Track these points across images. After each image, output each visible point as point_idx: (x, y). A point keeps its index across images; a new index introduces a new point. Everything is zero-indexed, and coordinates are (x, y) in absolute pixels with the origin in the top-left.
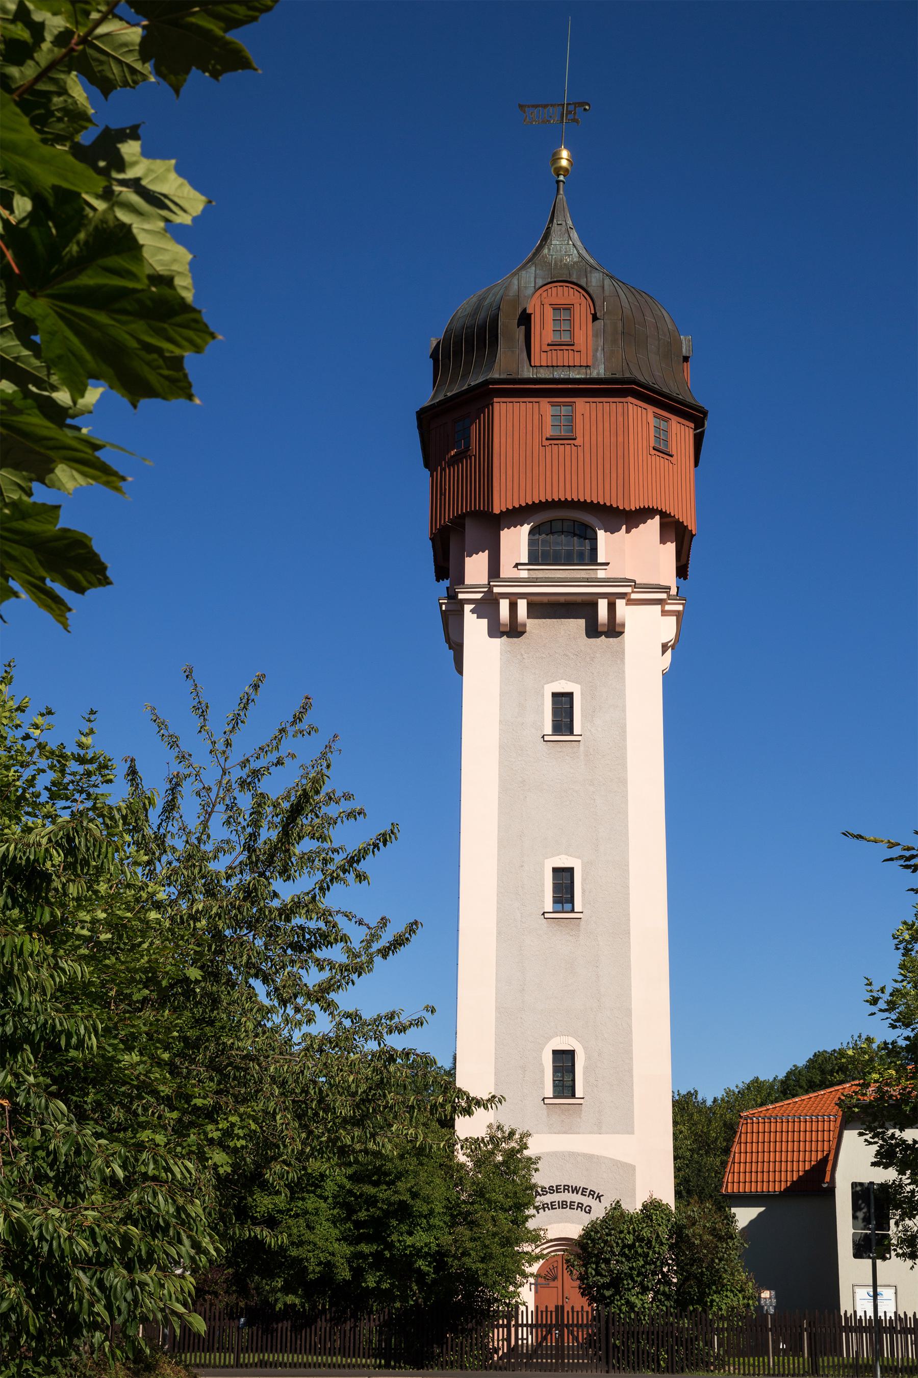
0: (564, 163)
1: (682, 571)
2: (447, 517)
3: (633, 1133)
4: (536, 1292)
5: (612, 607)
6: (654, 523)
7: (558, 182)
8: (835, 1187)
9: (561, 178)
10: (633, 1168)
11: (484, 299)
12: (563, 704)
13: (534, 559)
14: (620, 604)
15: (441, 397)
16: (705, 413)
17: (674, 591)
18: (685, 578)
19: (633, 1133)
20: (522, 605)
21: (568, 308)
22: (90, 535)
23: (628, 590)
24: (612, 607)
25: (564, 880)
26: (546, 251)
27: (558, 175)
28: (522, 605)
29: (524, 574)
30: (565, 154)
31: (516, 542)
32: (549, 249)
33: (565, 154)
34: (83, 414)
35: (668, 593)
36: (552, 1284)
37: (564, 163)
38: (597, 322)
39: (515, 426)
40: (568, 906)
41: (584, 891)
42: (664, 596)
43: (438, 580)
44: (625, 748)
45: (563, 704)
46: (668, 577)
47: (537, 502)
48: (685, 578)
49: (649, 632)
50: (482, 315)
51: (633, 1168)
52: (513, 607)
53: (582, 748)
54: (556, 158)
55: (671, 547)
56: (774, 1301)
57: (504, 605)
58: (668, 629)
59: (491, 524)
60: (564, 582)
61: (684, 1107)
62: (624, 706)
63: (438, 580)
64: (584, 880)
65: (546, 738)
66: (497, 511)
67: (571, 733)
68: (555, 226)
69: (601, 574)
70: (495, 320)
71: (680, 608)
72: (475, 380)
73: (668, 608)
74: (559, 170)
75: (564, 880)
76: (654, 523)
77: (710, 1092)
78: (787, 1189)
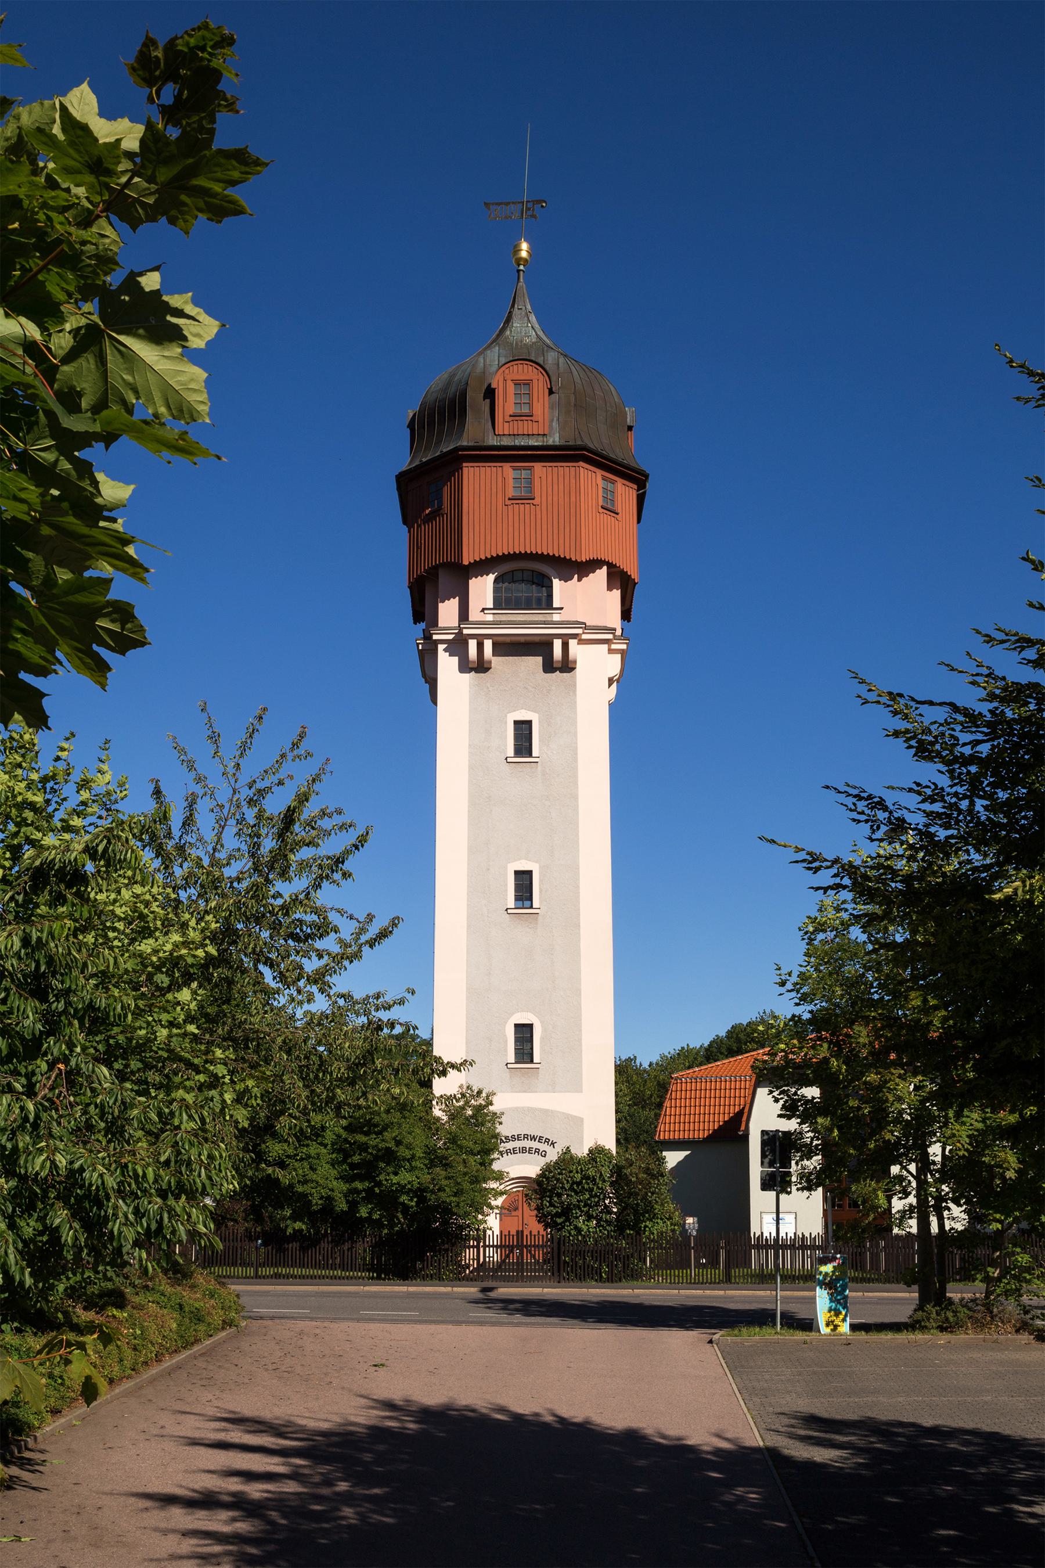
0: (524, 254)
2: (424, 566)
4: (501, 1220)
5: (565, 646)
7: (519, 271)
9: (522, 267)
12: (523, 730)
14: (573, 643)
15: (417, 463)
16: (647, 476)
17: (619, 632)
18: (629, 621)
20: (488, 645)
21: (528, 383)
23: (580, 631)
24: (565, 646)
26: (508, 333)
27: (519, 265)
28: (488, 645)
29: (490, 618)
30: (524, 246)
31: (482, 589)
33: (524, 246)
39: (481, 487)
40: (527, 903)
41: (541, 891)
43: (415, 623)
45: (523, 730)
46: (614, 620)
48: (629, 621)
49: (597, 667)
50: (453, 389)
54: (517, 250)
55: (617, 594)
57: (473, 644)
58: (613, 665)
60: (524, 624)
61: (624, 1071)
63: (415, 623)
64: (541, 881)
65: (509, 760)
66: (466, 562)
69: (556, 617)
71: (624, 647)
72: (446, 447)
73: (613, 646)
74: (519, 261)
77: (647, 1057)
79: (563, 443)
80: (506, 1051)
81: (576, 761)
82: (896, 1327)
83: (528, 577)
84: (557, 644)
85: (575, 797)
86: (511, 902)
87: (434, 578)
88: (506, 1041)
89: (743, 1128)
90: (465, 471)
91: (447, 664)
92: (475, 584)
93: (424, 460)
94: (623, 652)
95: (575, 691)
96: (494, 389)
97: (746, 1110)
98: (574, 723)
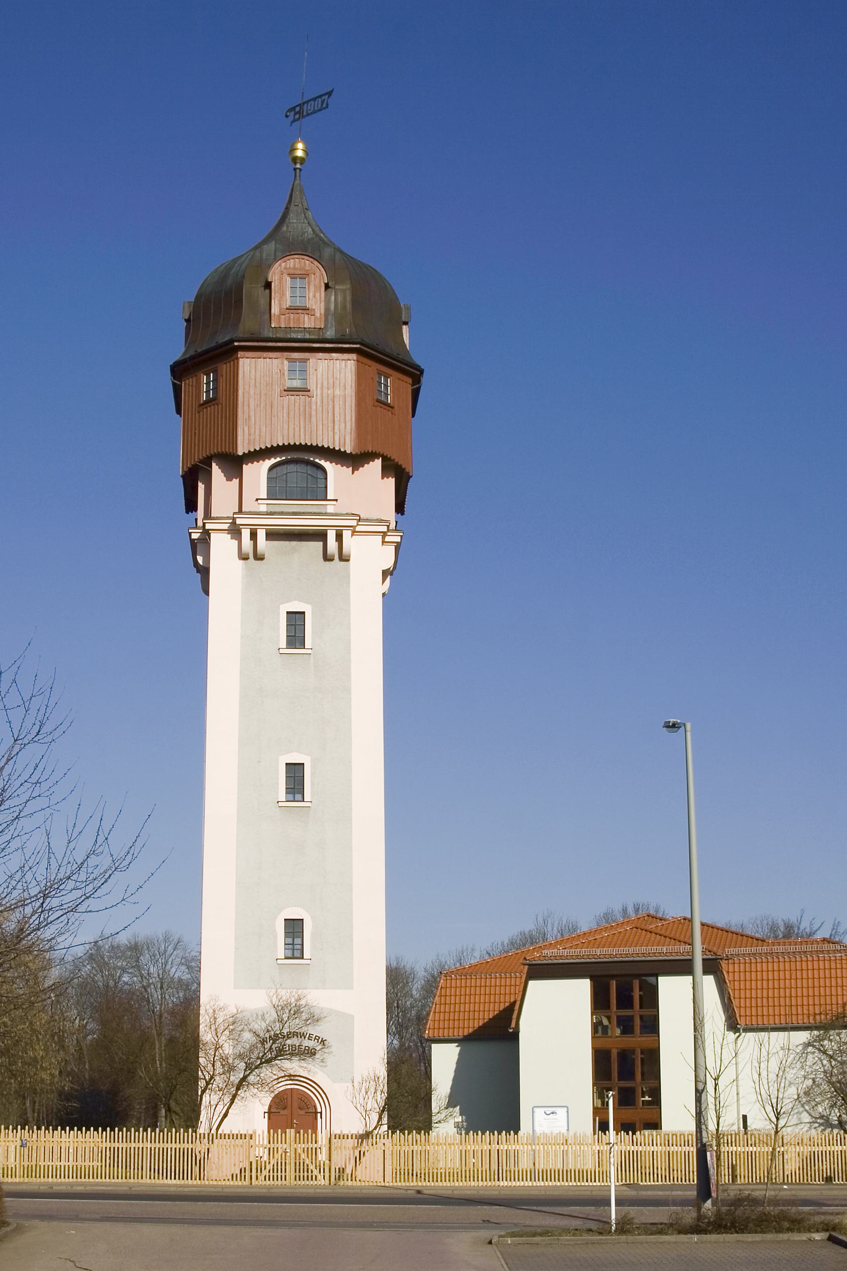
0: (300, 153)
1: (400, 508)
2: (196, 458)
3: (352, 988)
4: (269, 1118)
5: (339, 537)
6: (378, 463)
7: (295, 169)
8: (518, 1032)
9: (298, 166)
10: (352, 1017)
11: (231, 268)
12: (296, 620)
13: (272, 495)
14: (346, 534)
15: (191, 353)
16: (422, 372)
17: (392, 526)
18: (403, 514)
19: (352, 988)
20: (261, 534)
21: (304, 276)
22: (529, 926)
23: (354, 523)
24: (339, 537)
25: (295, 773)
26: (284, 228)
27: (295, 163)
28: (261, 534)
29: (263, 508)
30: (300, 146)
31: (257, 474)
32: (288, 227)
33: (300, 146)
34: (797, 1224)
35: (388, 526)
36: (282, 1112)
37: (300, 153)
38: (329, 290)
39: (255, 372)
40: (298, 797)
41: (312, 784)
42: (384, 529)
43: (187, 512)
44: (350, 661)
45: (296, 620)
46: (390, 514)
47: (275, 445)
48: (403, 514)
49: (371, 556)
50: (230, 281)
51: (352, 1017)
52: (254, 535)
53: (312, 660)
54: (293, 149)
55: (391, 482)
56: (465, 1124)
57: (246, 534)
58: (387, 558)
59: (234, 464)
60: (298, 515)
61: (396, 978)
62: (349, 624)
63: (187, 512)
64: (313, 774)
65: (281, 651)
66: (240, 453)
67: (303, 646)
68: (292, 207)
69: (330, 509)
70: (239, 288)
71: (398, 539)
72: (223, 338)
73: (387, 539)
74: (295, 159)
75: (295, 773)
76: (378, 463)
77: (420, 963)
78: (475, 1032)
79: (339, 336)
80: (276, 946)
81: (349, 653)
82: (416, 394)
83: (301, 465)
84: (331, 536)
85: (347, 690)
86: (282, 794)
87: (213, 453)
88: (276, 937)
89: (513, 1025)
90: (241, 361)
91: (222, 549)
92: (248, 469)
93: (199, 350)
94: (398, 547)
95: (349, 582)
96: (271, 283)
97: (517, 1007)
98: (347, 600)
